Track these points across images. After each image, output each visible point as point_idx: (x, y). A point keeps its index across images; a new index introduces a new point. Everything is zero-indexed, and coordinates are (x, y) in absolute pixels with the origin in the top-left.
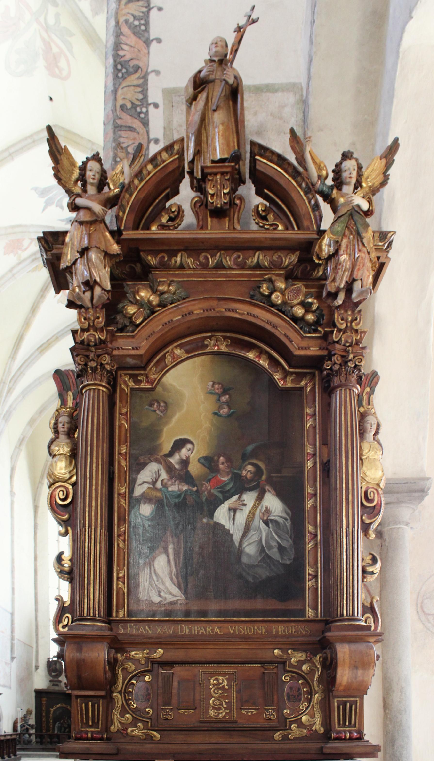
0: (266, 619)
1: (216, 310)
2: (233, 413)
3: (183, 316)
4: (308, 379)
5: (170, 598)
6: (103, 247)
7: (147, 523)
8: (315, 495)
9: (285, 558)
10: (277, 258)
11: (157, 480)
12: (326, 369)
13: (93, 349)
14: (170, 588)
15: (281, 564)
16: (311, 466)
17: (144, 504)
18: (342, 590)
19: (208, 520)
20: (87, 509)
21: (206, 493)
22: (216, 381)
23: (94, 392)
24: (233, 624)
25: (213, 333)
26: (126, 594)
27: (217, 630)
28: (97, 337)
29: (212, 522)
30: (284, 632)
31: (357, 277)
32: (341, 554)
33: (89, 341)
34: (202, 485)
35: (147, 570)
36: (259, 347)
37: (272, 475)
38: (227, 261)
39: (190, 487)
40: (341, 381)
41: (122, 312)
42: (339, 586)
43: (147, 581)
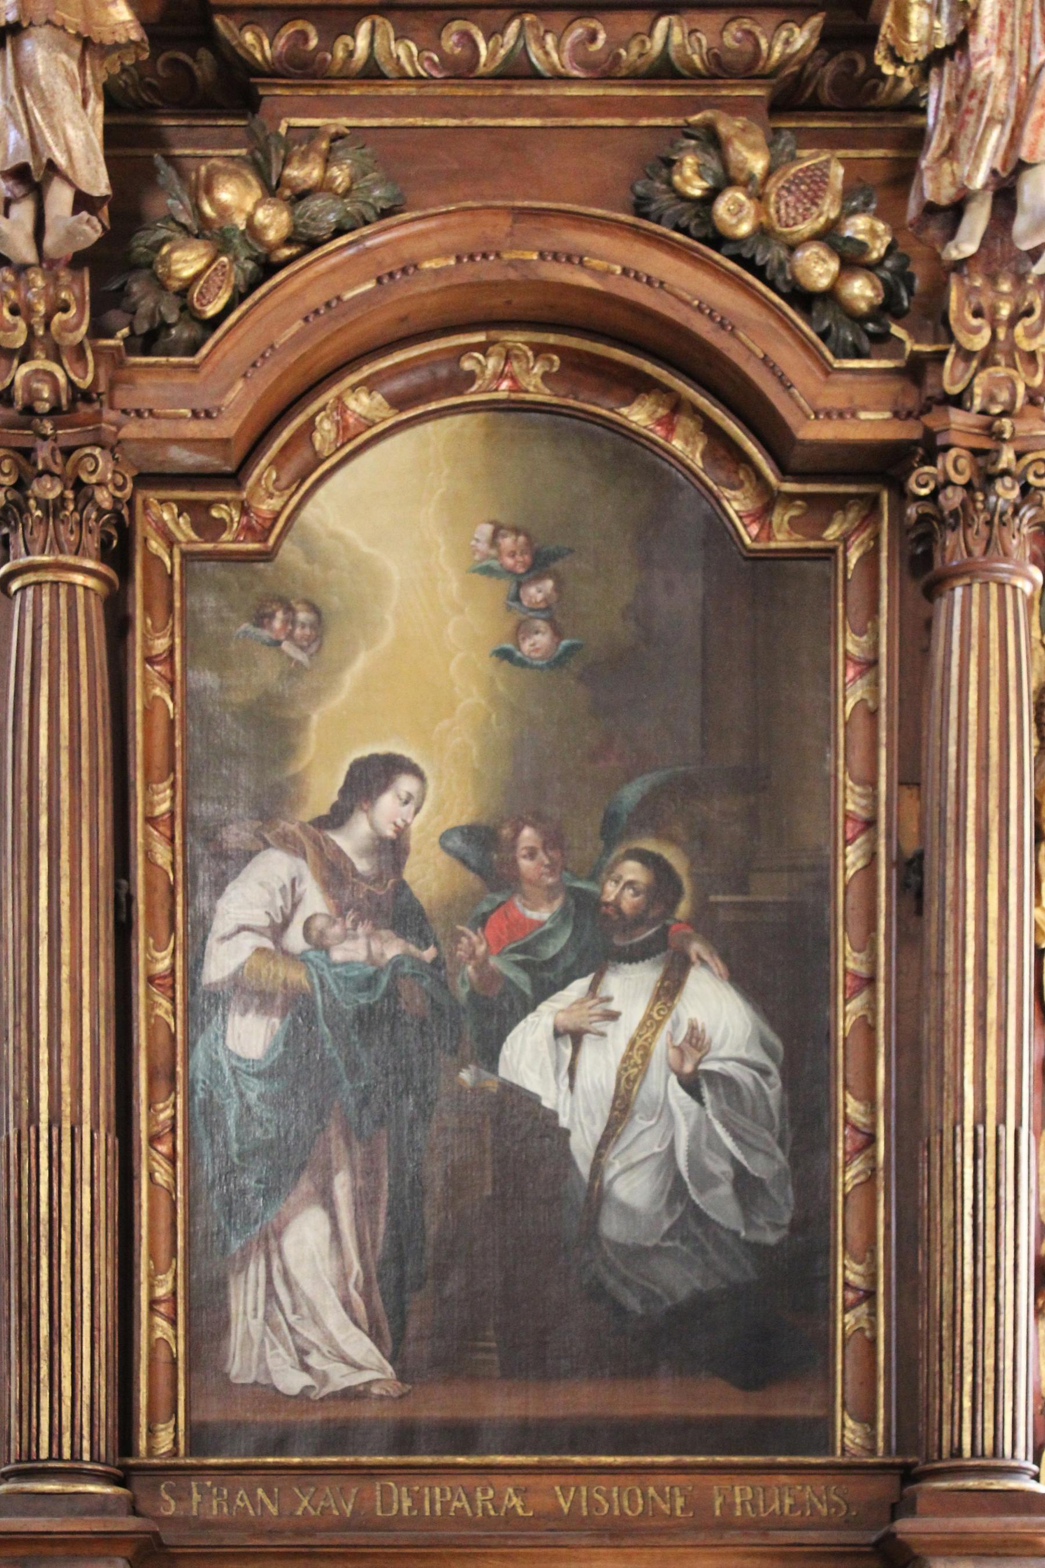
0: (688, 1459)
1: (506, 256)
2: (570, 650)
3: (379, 280)
4: (851, 515)
5: (342, 1378)
6: (74, 21)
7: (254, 1090)
8: (871, 981)
9: (761, 1221)
10: (738, 41)
11: (287, 922)
12: (918, 498)
13: (48, 428)
14: (339, 1337)
15: (747, 1243)
16: (860, 864)
17: (244, 1013)
18: (958, 1357)
19: (478, 1074)
20: (44, 1055)
21: (470, 968)
22: (503, 519)
23: (55, 596)
24: (571, 1479)
25: (494, 334)
26: (181, 1364)
27: (515, 1500)
28: (62, 380)
29: (493, 1086)
30: (755, 1507)
31: (1032, 152)
32: (956, 1221)
33: (33, 396)
34: (456, 937)
35: (256, 1270)
36: (667, 390)
37: (712, 898)
38: (547, 54)
39: (413, 949)
40: (970, 553)
41: (150, 265)
42: (947, 1344)
43: (255, 1309)
